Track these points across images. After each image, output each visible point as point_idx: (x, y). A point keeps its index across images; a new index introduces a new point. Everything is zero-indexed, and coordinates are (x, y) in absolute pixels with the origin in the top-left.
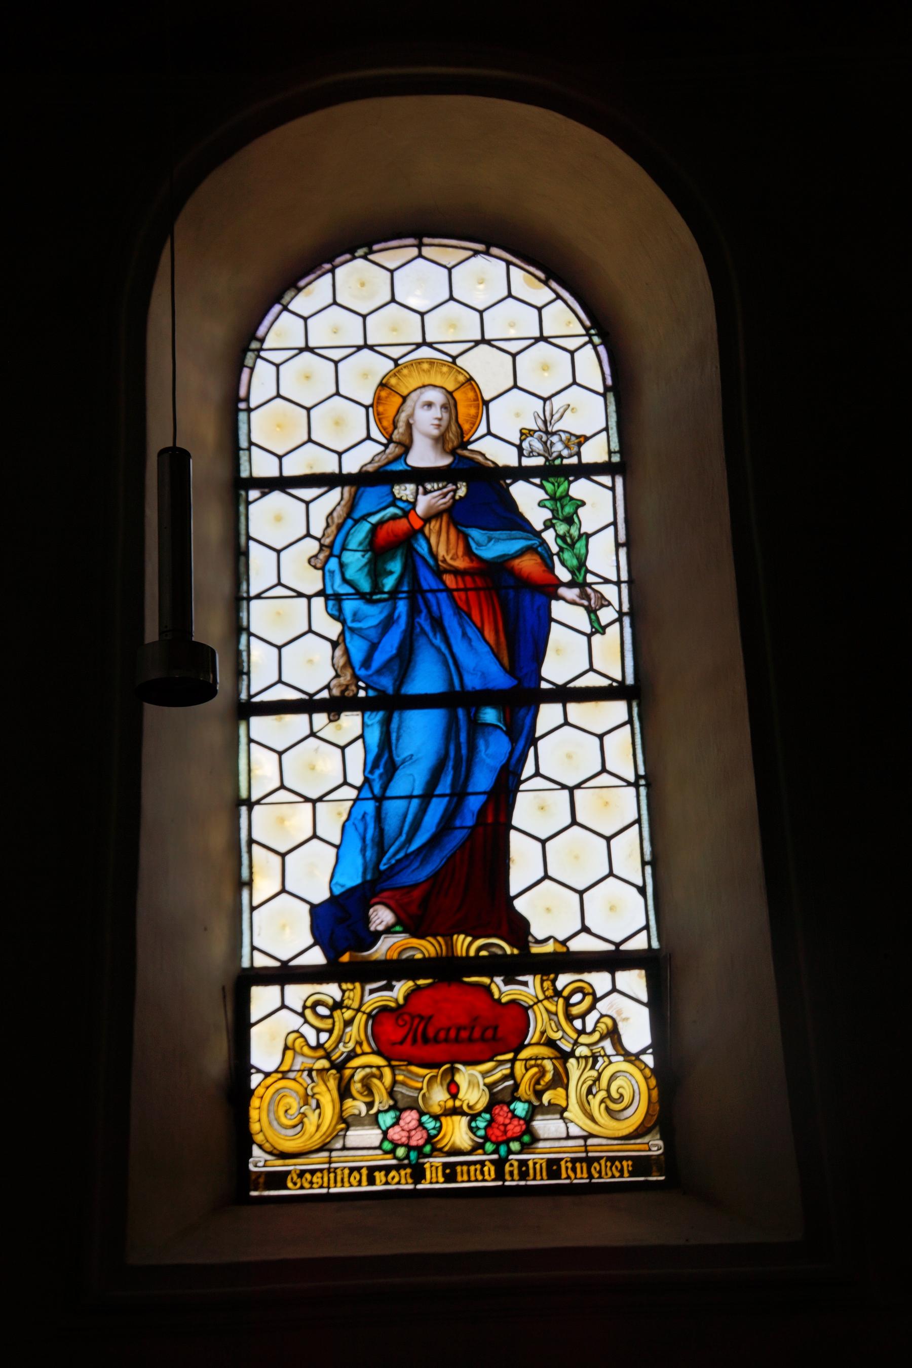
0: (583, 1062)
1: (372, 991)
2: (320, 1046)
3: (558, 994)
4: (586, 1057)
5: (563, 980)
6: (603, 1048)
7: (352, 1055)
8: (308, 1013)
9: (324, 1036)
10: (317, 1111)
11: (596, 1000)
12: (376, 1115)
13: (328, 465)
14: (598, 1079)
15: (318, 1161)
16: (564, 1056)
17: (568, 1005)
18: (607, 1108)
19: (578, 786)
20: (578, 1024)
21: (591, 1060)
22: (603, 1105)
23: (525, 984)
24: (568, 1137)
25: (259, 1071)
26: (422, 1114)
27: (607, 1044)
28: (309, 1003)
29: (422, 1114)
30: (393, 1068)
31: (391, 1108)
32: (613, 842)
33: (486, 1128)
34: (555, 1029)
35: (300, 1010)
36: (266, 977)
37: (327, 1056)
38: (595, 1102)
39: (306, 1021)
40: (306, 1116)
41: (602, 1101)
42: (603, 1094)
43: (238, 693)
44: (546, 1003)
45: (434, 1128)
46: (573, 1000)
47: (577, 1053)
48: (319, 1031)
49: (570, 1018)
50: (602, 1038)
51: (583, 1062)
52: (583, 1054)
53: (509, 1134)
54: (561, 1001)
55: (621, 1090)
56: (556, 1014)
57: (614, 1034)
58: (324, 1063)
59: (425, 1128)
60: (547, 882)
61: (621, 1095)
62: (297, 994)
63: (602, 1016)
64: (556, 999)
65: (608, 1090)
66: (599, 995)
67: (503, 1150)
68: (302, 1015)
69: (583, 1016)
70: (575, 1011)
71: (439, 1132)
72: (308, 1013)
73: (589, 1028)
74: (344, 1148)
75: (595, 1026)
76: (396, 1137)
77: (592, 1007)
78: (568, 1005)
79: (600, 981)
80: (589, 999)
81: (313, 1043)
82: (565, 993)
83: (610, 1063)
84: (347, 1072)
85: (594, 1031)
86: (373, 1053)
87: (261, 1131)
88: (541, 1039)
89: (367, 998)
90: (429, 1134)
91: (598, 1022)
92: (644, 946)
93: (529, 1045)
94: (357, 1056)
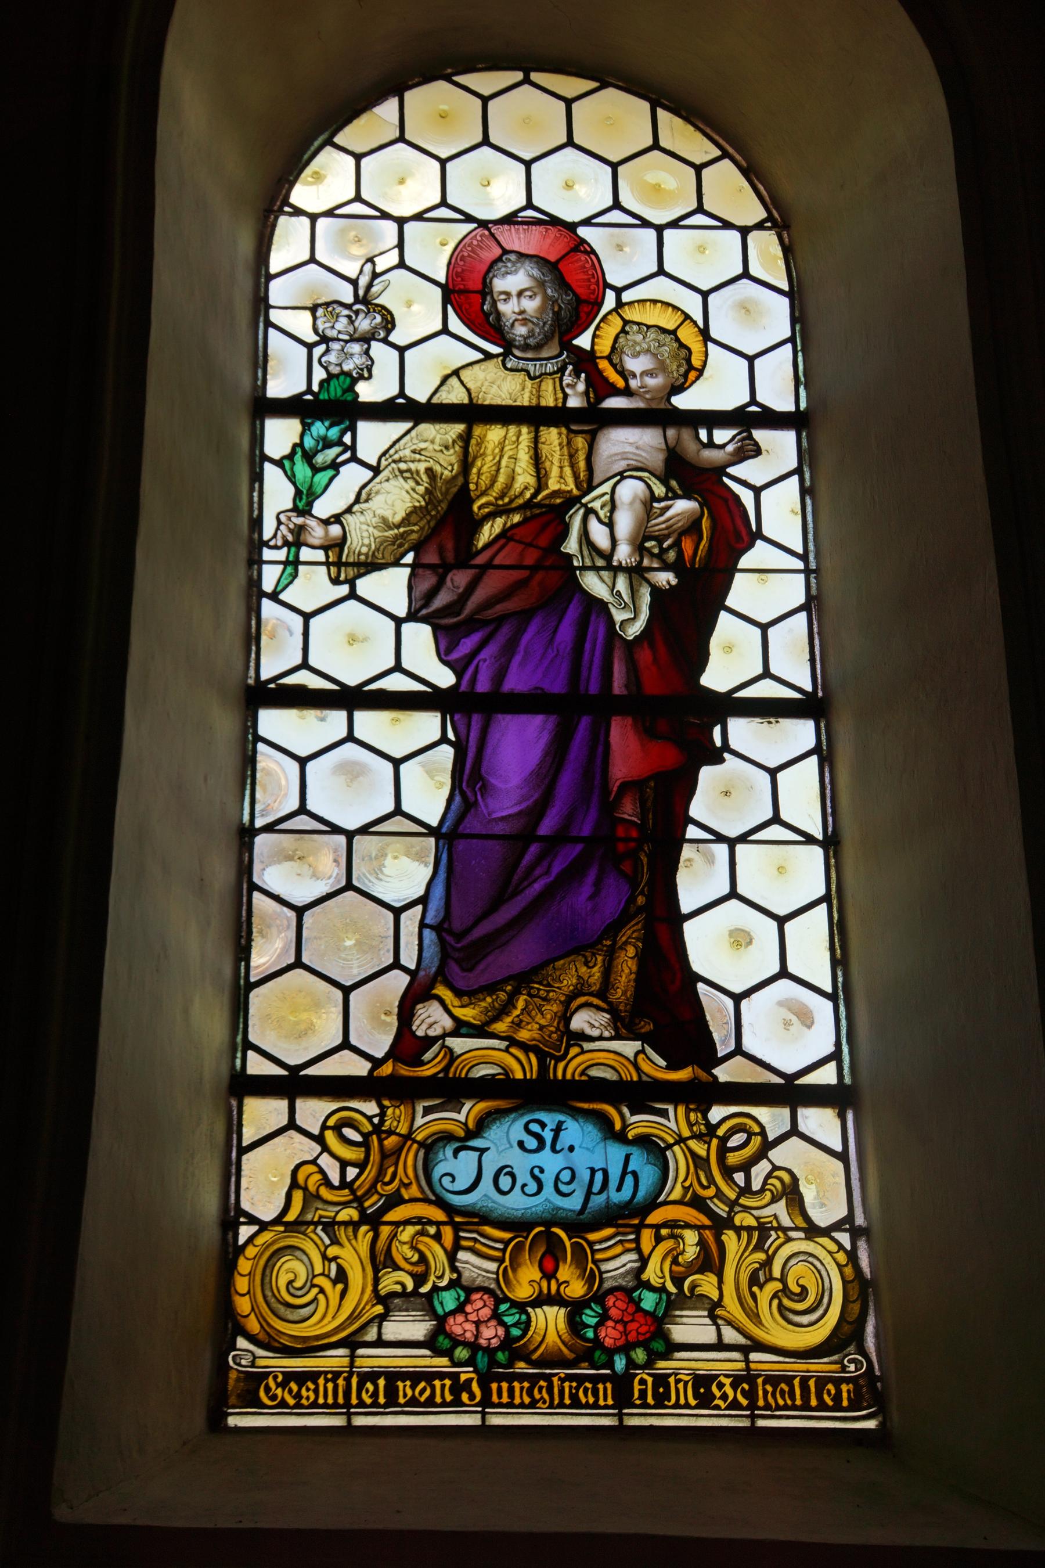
0: (744, 1235)
1: (427, 1111)
2: (344, 1184)
3: (712, 1129)
4: (749, 1229)
5: (717, 1113)
6: (775, 1216)
7: (395, 1200)
8: (330, 1137)
9: (352, 1172)
10: (340, 1286)
11: (767, 1146)
12: (429, 1296)
13: (371, 724)
14: (768, 1262)
15: (336, 1359)
16: (721, 1224)
17: (723, 1151)
18: (780, 1306)
19: (743, 838)
20: (739, 1177)
21: (756, 1234)
22: (775, 1302)
23: (664, 1113)
24: (720, 1346)
25: (252, 1220)
26: (498, 1301)
27: (780, 1208)
28: (331, 1122)
29: (498, 1301)
30: (457, 1228)
31: (453, 1284)
32: (776, 968)
33: (596, 1327)
34: (705, 1183)
35: (316, 1131)
36: (265, 1087)
37: (358, 1201)
38: (764, 1295)
39: (325, 1149)
40: (367, 314)
41: (775, 1296)
42: (774, 1286)
43: (246, 677)
44: (692, 1143)
45: (515, 1325)
46: (732, 1143)
47: (737, 1220)
48: (344, 1164)
49: (728, 1172)
50: (774, 1200)
51: (744, 1235)
52: (745, 1224)
53: (632, 1337)
54: (715, 1142)
55: (801, 1282)
56: (707, 1160)
57: (792, 1194)
58: (350, 1213)
59: (502, 1323)
60: (771, 631)
61: (804, 1289)
62: (313, 1112)
63: (775, 1168)
64: (707, 1139)
65: (783, 1280)
66: (771, 1137)
67: (620, 1363)
68: (320, 1139)
69: (746, 1167)
70: (732, 1159)
71: (525, 1331)
72: (330, 1137)
73: (756, 1186)
74: (380, 1343)
75: (765, 1183)
76: (458, 1330)
77: (762, 1154)
78: (723, 1151)
79: (772, 1118)
80: (757, 1141)
81: (335, 1179)
82: (720, 1132)
83: (789, 1240)
84: (385, 1231)
85: (762, 1190)
86: (425, 1200)
87: (249, 1292)
88: (684, 1195)
89: (419, 1121)
90: (507, 1332)
91: (769, 1176)
92: (833, 1080)
93: (666, 1203)
94: (401, 1201)
